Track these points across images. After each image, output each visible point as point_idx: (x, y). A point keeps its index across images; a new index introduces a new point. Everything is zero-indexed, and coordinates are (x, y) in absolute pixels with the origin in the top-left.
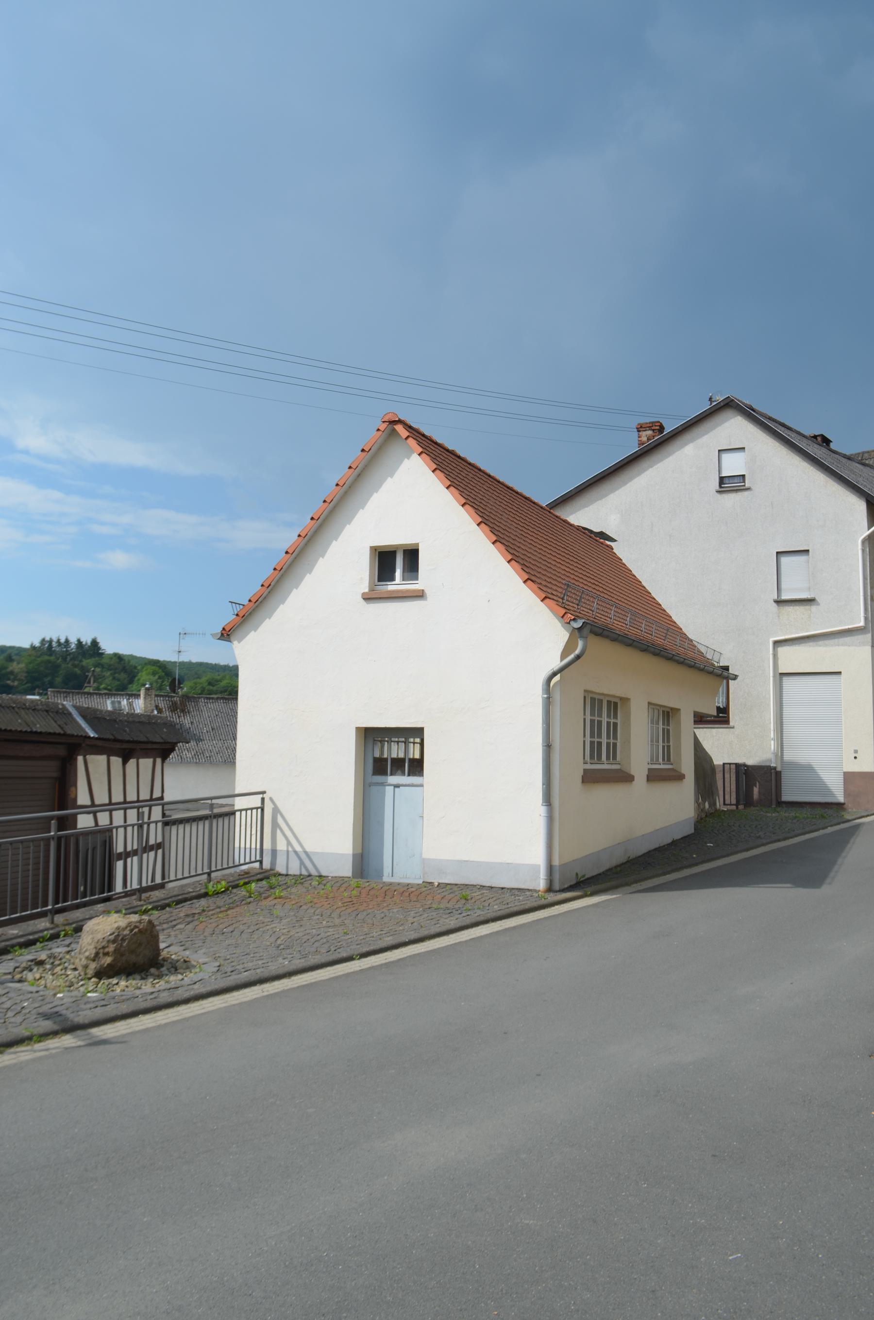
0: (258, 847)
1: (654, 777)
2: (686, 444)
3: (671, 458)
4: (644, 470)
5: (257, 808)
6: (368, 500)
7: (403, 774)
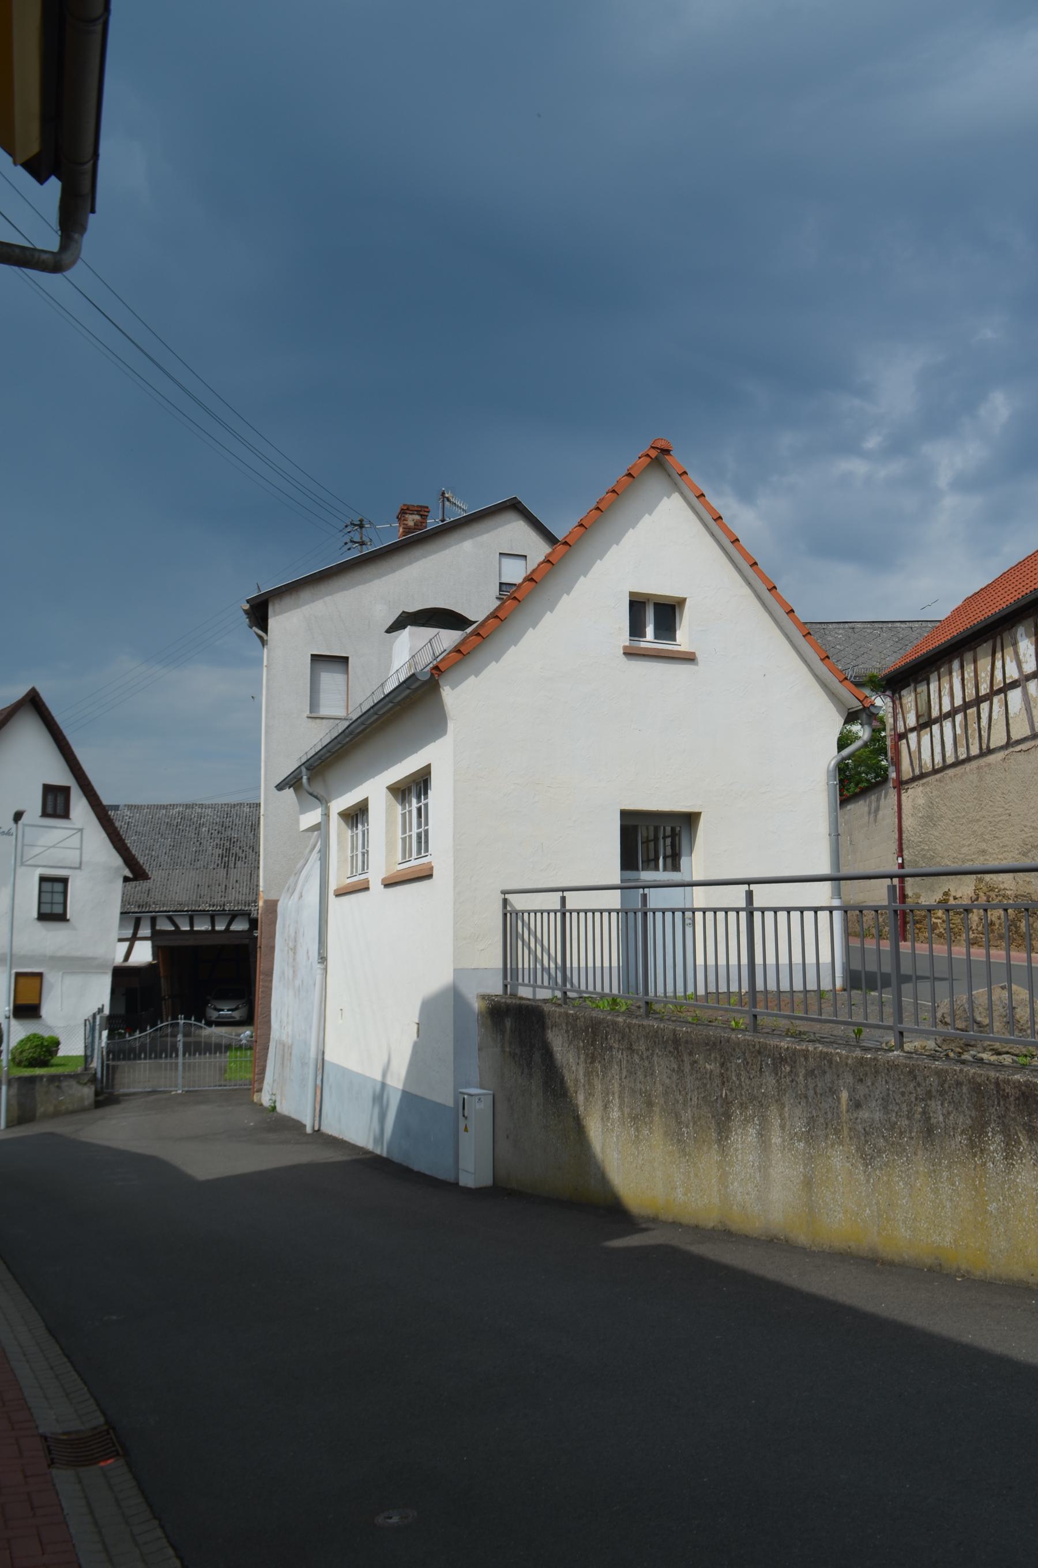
0: (744, 960)
1: (694, 911)
2: (464, 539)
3: (447, 551)
4: (417, 559)
5: (737, 911)
6: (624, 535)
7: (657, 868)
